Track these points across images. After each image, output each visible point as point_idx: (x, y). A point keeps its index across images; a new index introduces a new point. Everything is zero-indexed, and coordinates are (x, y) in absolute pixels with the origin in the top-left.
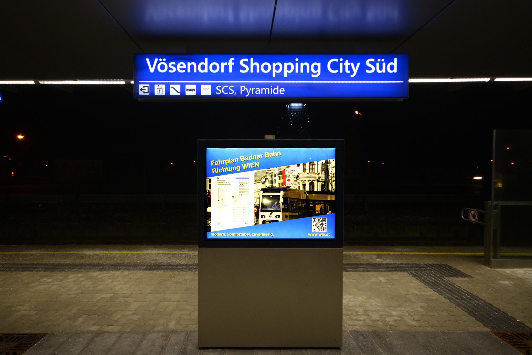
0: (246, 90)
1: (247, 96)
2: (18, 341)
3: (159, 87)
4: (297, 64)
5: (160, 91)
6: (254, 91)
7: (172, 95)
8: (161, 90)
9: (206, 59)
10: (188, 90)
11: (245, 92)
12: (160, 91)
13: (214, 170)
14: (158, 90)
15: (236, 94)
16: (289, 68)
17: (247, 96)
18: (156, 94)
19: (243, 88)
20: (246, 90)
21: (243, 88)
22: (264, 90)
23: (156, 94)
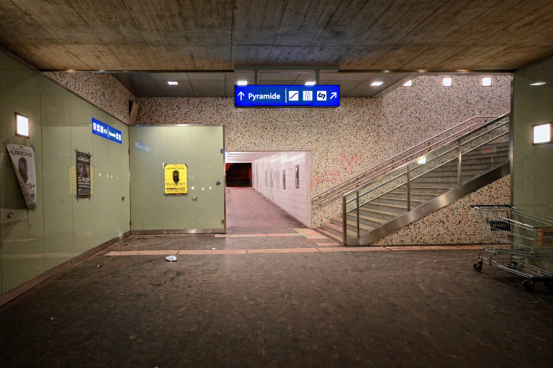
0: (253, 96)
1: (253, 100)
2: (478, 159)
3: (308, 94)
4: (271, 95)
5: (308, 97)
6: (259, 97)
7: (299, 99)
8: (309, 96)
9: (275, 94)
10: (406, 194)
11: (252, 98)
12: (308, 97)
13: (508, 198)
14: (307, 96)
15: (242, 99)
16: (274, 97)
17: (253, 100)
18: (304, 99)
19: (250, 95)
20: (253, 96)
21: (250, 95)
22: (265, 97)
23: (304, 99)
